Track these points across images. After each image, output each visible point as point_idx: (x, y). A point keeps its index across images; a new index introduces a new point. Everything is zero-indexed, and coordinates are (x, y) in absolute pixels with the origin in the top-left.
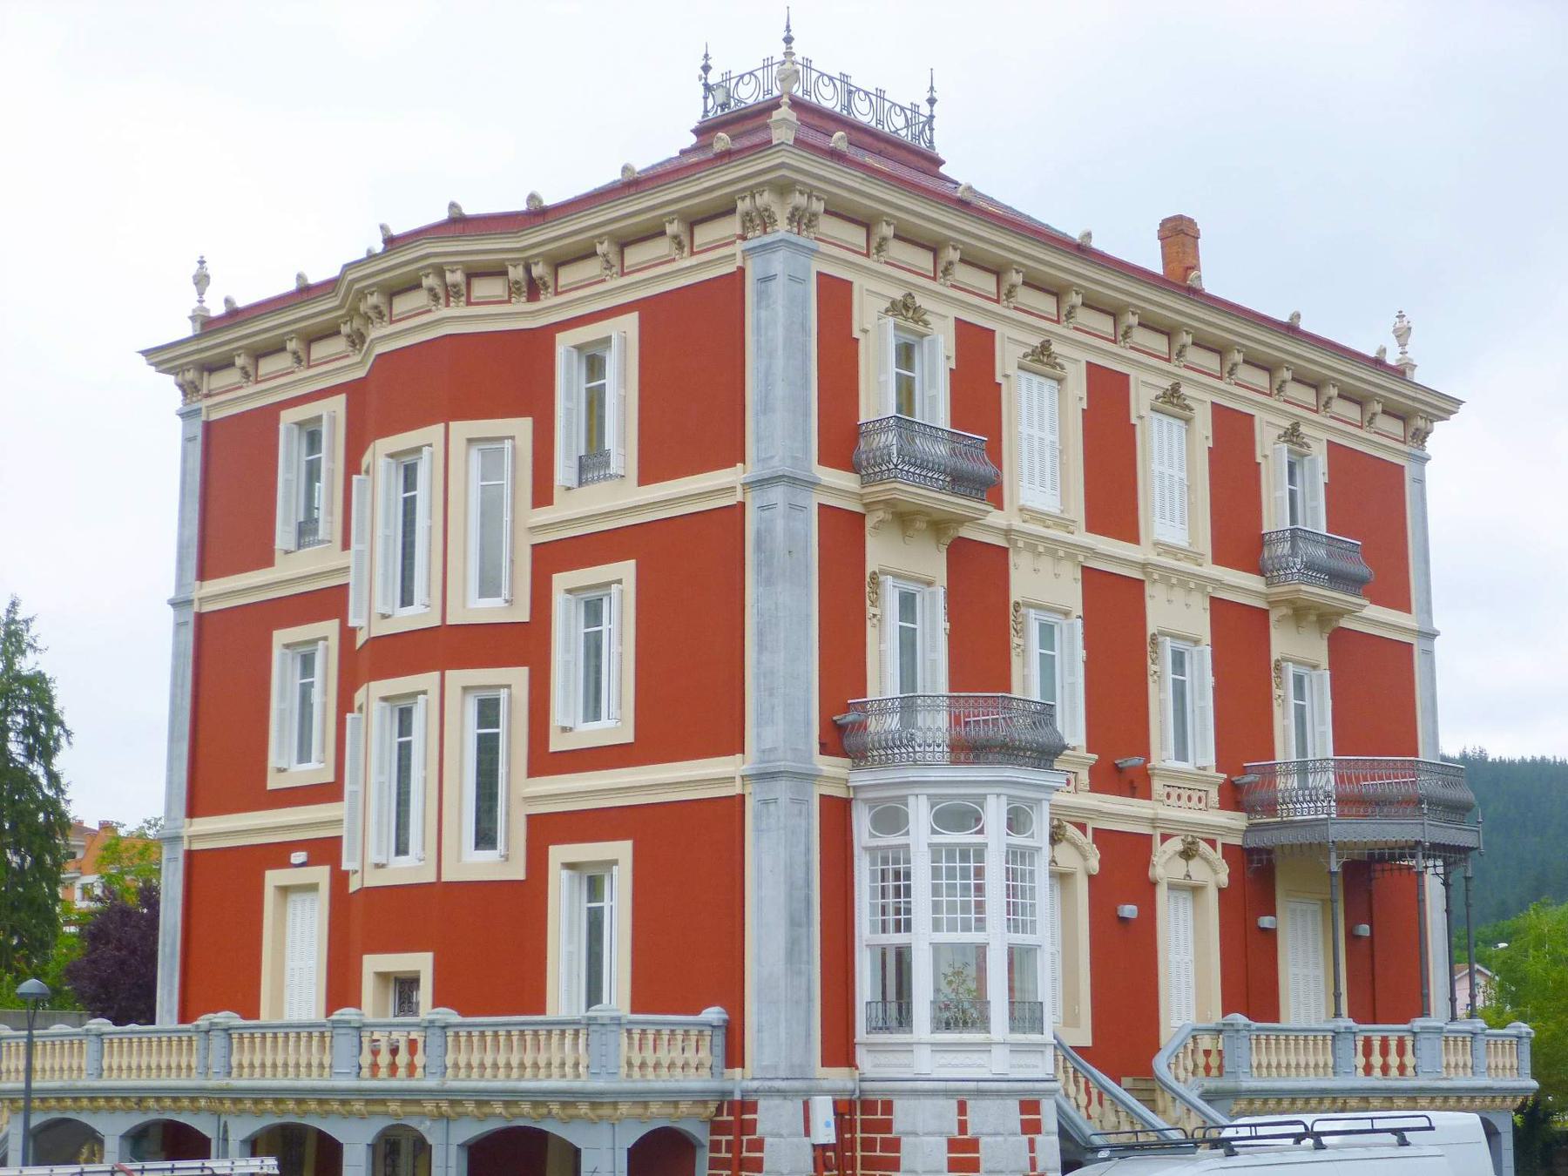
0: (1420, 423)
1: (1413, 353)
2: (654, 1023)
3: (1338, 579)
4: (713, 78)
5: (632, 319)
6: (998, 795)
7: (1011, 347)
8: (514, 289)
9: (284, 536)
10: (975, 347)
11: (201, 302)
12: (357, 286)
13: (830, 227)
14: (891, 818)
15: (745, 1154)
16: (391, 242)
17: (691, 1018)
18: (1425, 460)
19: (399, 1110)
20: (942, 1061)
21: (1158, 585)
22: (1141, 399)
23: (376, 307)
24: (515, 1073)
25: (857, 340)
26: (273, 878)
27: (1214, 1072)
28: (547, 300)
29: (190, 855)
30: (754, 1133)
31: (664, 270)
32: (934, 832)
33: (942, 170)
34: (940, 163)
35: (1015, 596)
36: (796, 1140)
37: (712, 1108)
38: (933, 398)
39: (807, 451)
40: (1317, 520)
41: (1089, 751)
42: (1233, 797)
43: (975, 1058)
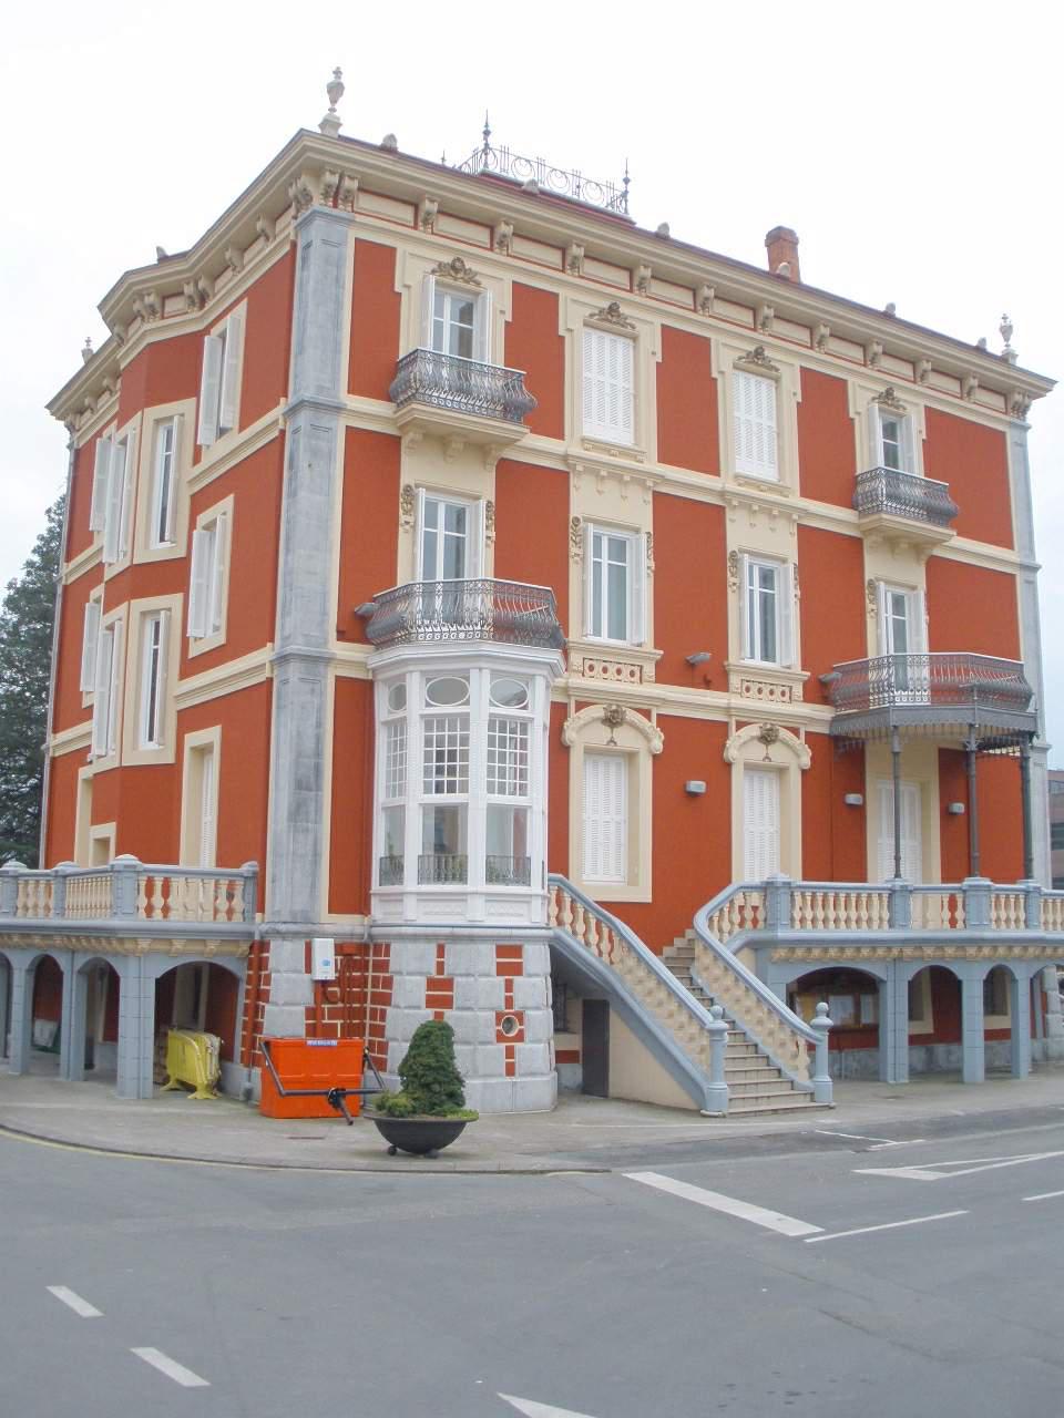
0: (1018, 397)
1: (1016, 344)
3: (935, 514)
6: (480, 669)
7: (724, 352)
11: (332, 110)
12: (135, 288)
14: (399, 699)
15: (262, 987)
16: (164, 259)
17: (234, 871)
18: (1026, 428)
19: (41, 943)
22: (723, 358)
23: (152, 306)
24: (41, 912)
25: (715, 380)
27: (761, 924)
30: (267, 969)
32: (428, 705)
35: (574, 512)
36: (294, 976)
37: (245, 947)
40: (913, 462)
42: (819, 691)
43: (454, 907)
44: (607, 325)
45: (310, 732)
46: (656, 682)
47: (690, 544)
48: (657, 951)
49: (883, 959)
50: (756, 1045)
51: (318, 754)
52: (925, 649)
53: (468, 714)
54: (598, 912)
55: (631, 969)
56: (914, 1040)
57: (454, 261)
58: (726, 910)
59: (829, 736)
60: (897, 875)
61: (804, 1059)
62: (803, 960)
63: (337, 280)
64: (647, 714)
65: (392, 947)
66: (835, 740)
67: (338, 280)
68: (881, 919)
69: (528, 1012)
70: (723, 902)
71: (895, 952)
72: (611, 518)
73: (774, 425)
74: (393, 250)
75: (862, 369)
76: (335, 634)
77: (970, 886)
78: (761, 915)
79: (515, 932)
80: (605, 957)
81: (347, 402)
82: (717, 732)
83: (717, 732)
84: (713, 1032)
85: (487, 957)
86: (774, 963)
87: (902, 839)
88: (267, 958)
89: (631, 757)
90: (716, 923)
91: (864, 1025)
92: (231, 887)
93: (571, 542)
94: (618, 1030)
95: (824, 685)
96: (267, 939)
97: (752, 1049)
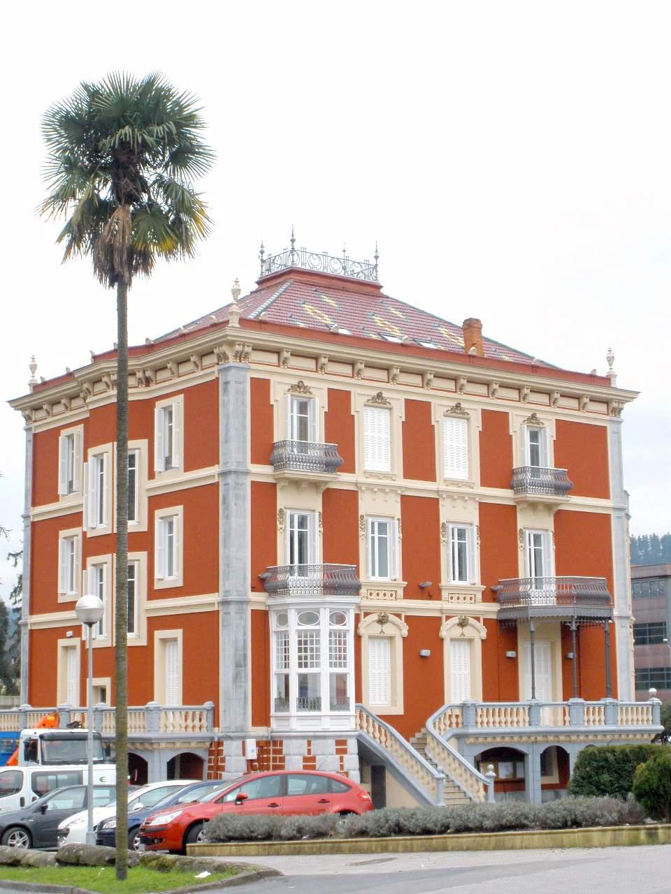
0: (615, 405)
1: (617, 368)
2: (503, 705)
4: (265, 257)
5: (182, 396)
8: (140, 381)
9: (62, 489)
10: (339, 403)
13: (256, 356)
14: (283, 619)
15: (219, 764)
16: (96, 358)
20: (302, 724)
21: (446, 500)
22: (437, 414)
26: (62, 643)
27: (460, 726)
28: (153, 387)
29: (31, 631)
31: (194, 377)
32: (299, 625)
33: (382, 290)
34: (380, 287)
36: (237, 758)
37: (208, 744)
38: (546, 454)
39: (245, 458)
40: (548, 460)
41: (403, 580)
42: (491, 595)
44: (376, 404)
45: (241, 638)
46: (404, 599)
47: (420, 519)
48: (408, 740)
49: (527, 742)
50: (459, 787)
51: (245, 648)
52: (553, 574)
53: (319, 630)
54: (380, 722)
55: (392, 747)
56: (544, 787)
57: (299, 383)
58: (442, 718)
59: (497, 620)
60: (533, 697)
61: (482, 792)
62: (482, 744)
63: (243, 403)
64: (399, 616)
65: (284, 743)
66: (501, 622)
67: (243, 403)
68: (524, 721)
69: (351, 772)
70: (441, 714)
71: (533, 738)
72: (380, 511)
73: (466, 446)
74: (429, 403)
75: (518, 404)
76: (250, 589)
77: (572, 703)
78: (460, 720)
79: (344, 733)
80: (383, 744)
81: (251, 469)
82: (435, 623)
83: (435, 623)
84: (438, 779)
85: (331, 746)
86: (468, 745)
87: (540, 675)
88: (222, 750)
89: (391, 638)
90: (437, 725)
91: (519, 779)
92: (201, 714)
93: (360, 529)
94: (390, 781)
95: (494, 592)
96: (222, 740)
97: (457, 789)
